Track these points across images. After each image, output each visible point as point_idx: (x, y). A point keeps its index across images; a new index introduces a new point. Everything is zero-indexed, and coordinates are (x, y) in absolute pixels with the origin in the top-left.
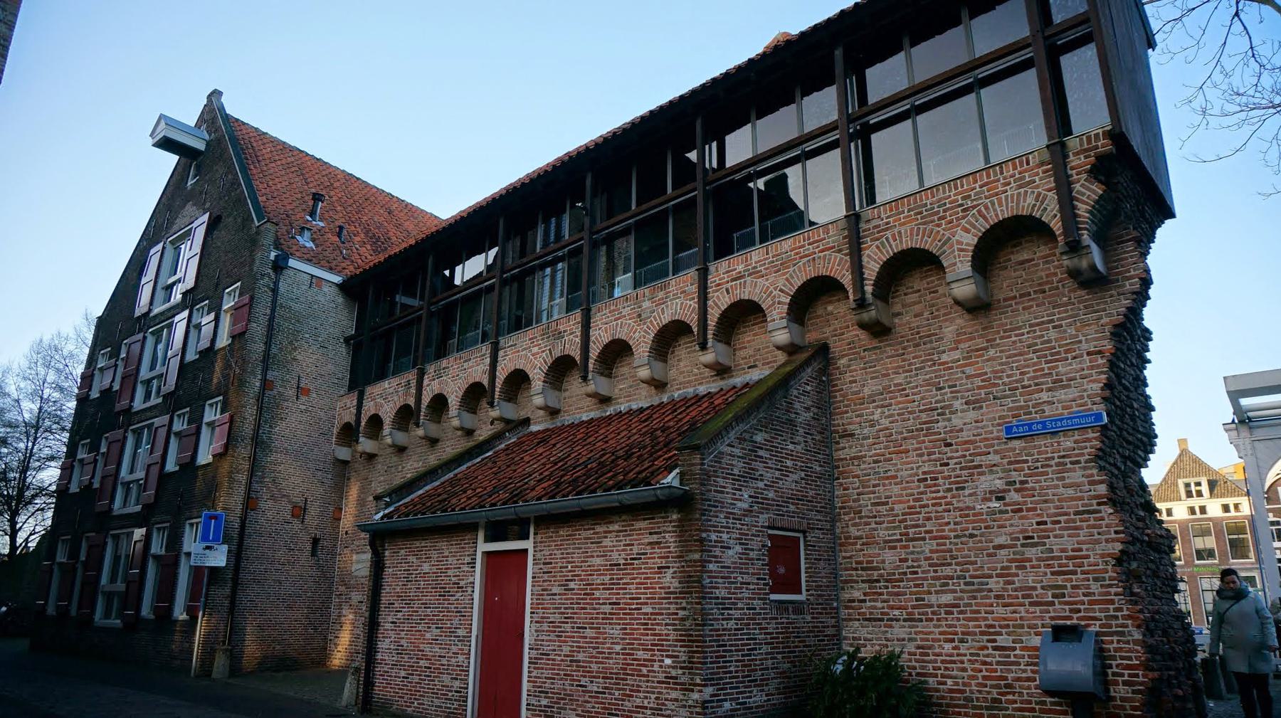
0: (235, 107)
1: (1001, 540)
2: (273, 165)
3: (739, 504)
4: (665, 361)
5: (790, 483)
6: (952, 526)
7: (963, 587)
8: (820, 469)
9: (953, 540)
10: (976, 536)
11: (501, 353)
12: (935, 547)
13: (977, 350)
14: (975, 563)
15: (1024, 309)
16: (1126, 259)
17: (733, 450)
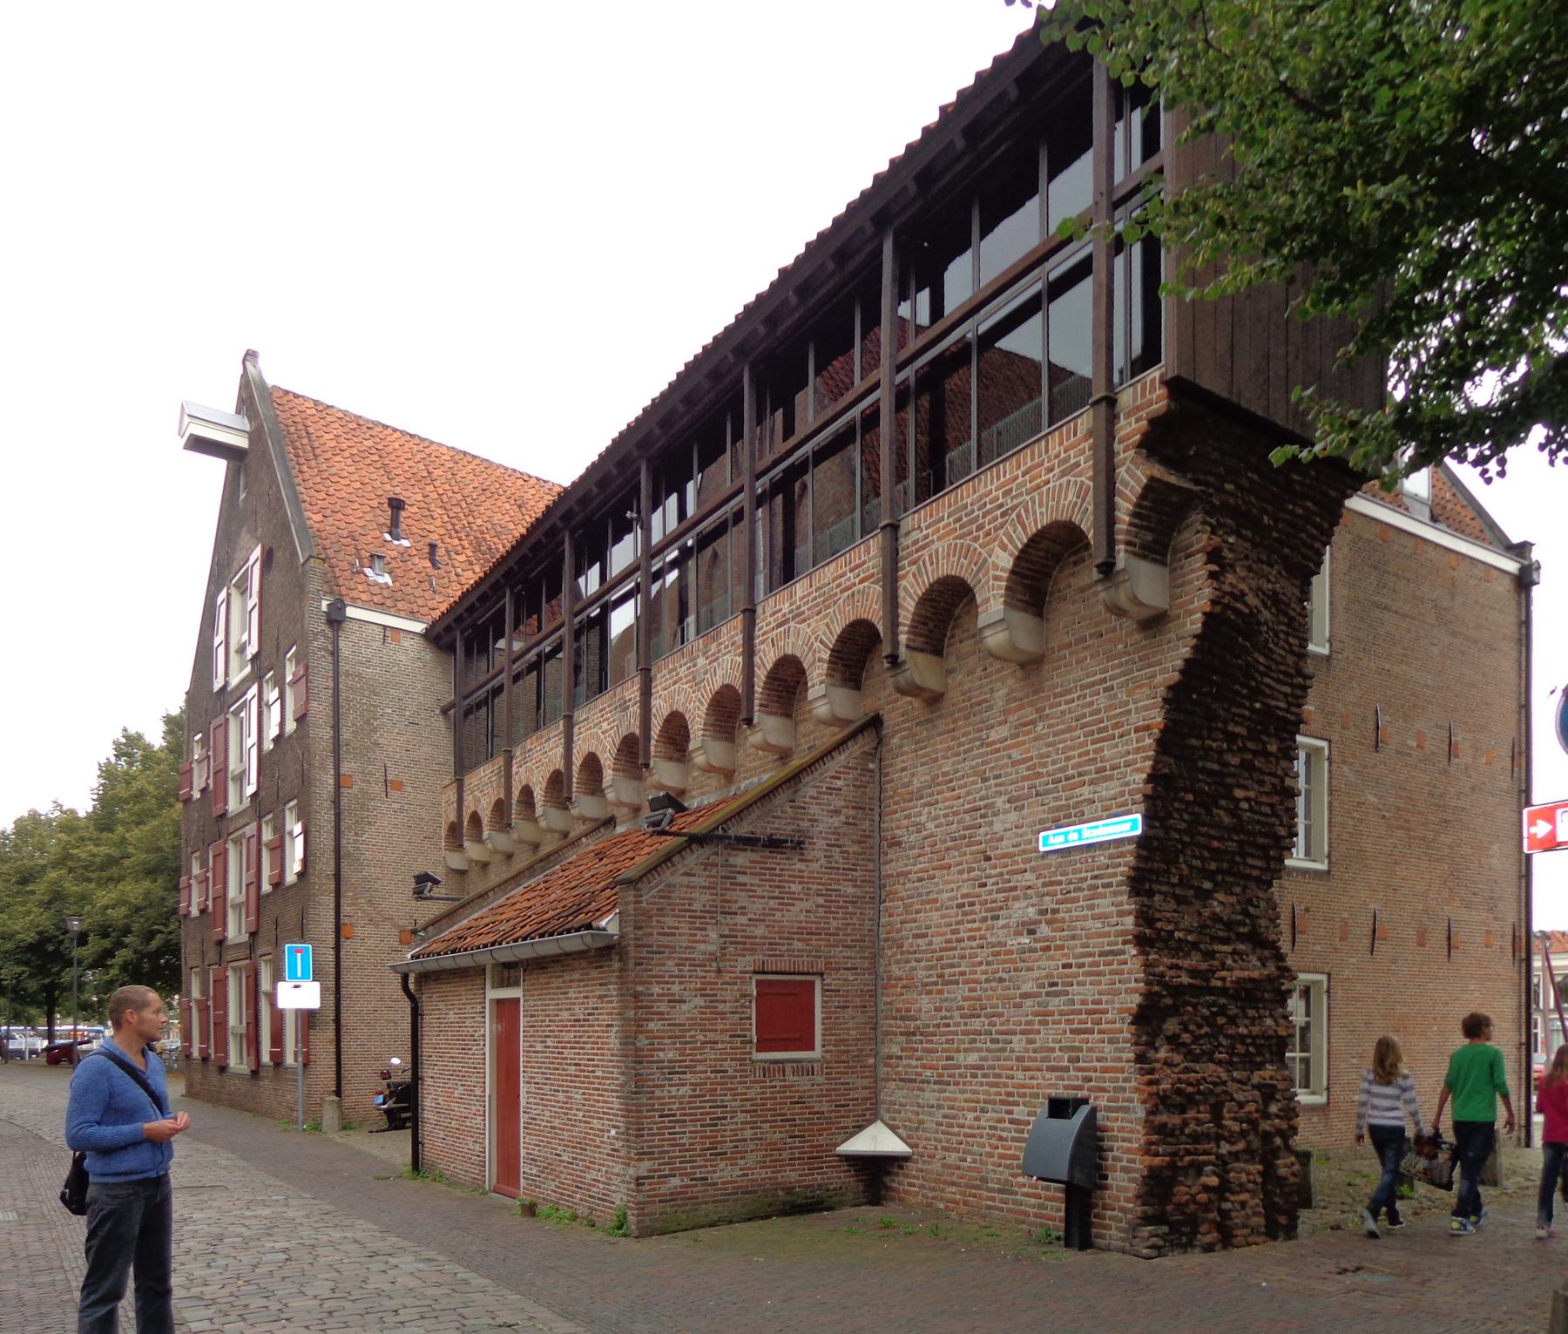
0: (274, 374)
1: (1028, 987)
2: (338, 458)
3: (702, 947)
4: (733, 741)
5: (796, 914)
6: (984, 967)
7: (989, 1045)
8: (854, 890)
9: (984, 985)
10: (1005, 980)
11: (576, 729)
12: (967, 994)
13: (1026, 724)
14: (1001, 1015)
15: (1077, 662)
16: (1190, 582)
17: (693, 879)
